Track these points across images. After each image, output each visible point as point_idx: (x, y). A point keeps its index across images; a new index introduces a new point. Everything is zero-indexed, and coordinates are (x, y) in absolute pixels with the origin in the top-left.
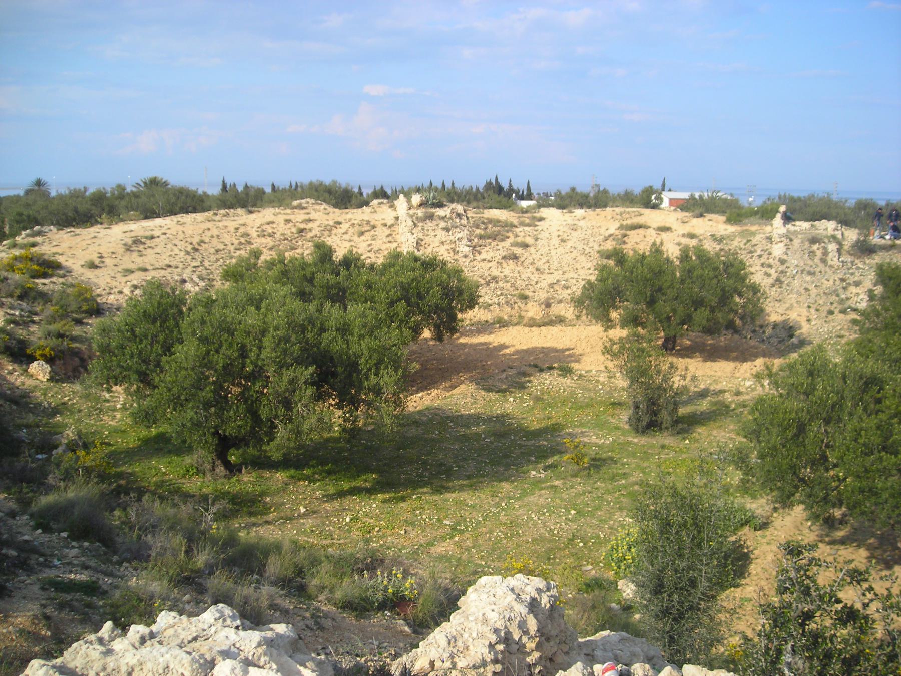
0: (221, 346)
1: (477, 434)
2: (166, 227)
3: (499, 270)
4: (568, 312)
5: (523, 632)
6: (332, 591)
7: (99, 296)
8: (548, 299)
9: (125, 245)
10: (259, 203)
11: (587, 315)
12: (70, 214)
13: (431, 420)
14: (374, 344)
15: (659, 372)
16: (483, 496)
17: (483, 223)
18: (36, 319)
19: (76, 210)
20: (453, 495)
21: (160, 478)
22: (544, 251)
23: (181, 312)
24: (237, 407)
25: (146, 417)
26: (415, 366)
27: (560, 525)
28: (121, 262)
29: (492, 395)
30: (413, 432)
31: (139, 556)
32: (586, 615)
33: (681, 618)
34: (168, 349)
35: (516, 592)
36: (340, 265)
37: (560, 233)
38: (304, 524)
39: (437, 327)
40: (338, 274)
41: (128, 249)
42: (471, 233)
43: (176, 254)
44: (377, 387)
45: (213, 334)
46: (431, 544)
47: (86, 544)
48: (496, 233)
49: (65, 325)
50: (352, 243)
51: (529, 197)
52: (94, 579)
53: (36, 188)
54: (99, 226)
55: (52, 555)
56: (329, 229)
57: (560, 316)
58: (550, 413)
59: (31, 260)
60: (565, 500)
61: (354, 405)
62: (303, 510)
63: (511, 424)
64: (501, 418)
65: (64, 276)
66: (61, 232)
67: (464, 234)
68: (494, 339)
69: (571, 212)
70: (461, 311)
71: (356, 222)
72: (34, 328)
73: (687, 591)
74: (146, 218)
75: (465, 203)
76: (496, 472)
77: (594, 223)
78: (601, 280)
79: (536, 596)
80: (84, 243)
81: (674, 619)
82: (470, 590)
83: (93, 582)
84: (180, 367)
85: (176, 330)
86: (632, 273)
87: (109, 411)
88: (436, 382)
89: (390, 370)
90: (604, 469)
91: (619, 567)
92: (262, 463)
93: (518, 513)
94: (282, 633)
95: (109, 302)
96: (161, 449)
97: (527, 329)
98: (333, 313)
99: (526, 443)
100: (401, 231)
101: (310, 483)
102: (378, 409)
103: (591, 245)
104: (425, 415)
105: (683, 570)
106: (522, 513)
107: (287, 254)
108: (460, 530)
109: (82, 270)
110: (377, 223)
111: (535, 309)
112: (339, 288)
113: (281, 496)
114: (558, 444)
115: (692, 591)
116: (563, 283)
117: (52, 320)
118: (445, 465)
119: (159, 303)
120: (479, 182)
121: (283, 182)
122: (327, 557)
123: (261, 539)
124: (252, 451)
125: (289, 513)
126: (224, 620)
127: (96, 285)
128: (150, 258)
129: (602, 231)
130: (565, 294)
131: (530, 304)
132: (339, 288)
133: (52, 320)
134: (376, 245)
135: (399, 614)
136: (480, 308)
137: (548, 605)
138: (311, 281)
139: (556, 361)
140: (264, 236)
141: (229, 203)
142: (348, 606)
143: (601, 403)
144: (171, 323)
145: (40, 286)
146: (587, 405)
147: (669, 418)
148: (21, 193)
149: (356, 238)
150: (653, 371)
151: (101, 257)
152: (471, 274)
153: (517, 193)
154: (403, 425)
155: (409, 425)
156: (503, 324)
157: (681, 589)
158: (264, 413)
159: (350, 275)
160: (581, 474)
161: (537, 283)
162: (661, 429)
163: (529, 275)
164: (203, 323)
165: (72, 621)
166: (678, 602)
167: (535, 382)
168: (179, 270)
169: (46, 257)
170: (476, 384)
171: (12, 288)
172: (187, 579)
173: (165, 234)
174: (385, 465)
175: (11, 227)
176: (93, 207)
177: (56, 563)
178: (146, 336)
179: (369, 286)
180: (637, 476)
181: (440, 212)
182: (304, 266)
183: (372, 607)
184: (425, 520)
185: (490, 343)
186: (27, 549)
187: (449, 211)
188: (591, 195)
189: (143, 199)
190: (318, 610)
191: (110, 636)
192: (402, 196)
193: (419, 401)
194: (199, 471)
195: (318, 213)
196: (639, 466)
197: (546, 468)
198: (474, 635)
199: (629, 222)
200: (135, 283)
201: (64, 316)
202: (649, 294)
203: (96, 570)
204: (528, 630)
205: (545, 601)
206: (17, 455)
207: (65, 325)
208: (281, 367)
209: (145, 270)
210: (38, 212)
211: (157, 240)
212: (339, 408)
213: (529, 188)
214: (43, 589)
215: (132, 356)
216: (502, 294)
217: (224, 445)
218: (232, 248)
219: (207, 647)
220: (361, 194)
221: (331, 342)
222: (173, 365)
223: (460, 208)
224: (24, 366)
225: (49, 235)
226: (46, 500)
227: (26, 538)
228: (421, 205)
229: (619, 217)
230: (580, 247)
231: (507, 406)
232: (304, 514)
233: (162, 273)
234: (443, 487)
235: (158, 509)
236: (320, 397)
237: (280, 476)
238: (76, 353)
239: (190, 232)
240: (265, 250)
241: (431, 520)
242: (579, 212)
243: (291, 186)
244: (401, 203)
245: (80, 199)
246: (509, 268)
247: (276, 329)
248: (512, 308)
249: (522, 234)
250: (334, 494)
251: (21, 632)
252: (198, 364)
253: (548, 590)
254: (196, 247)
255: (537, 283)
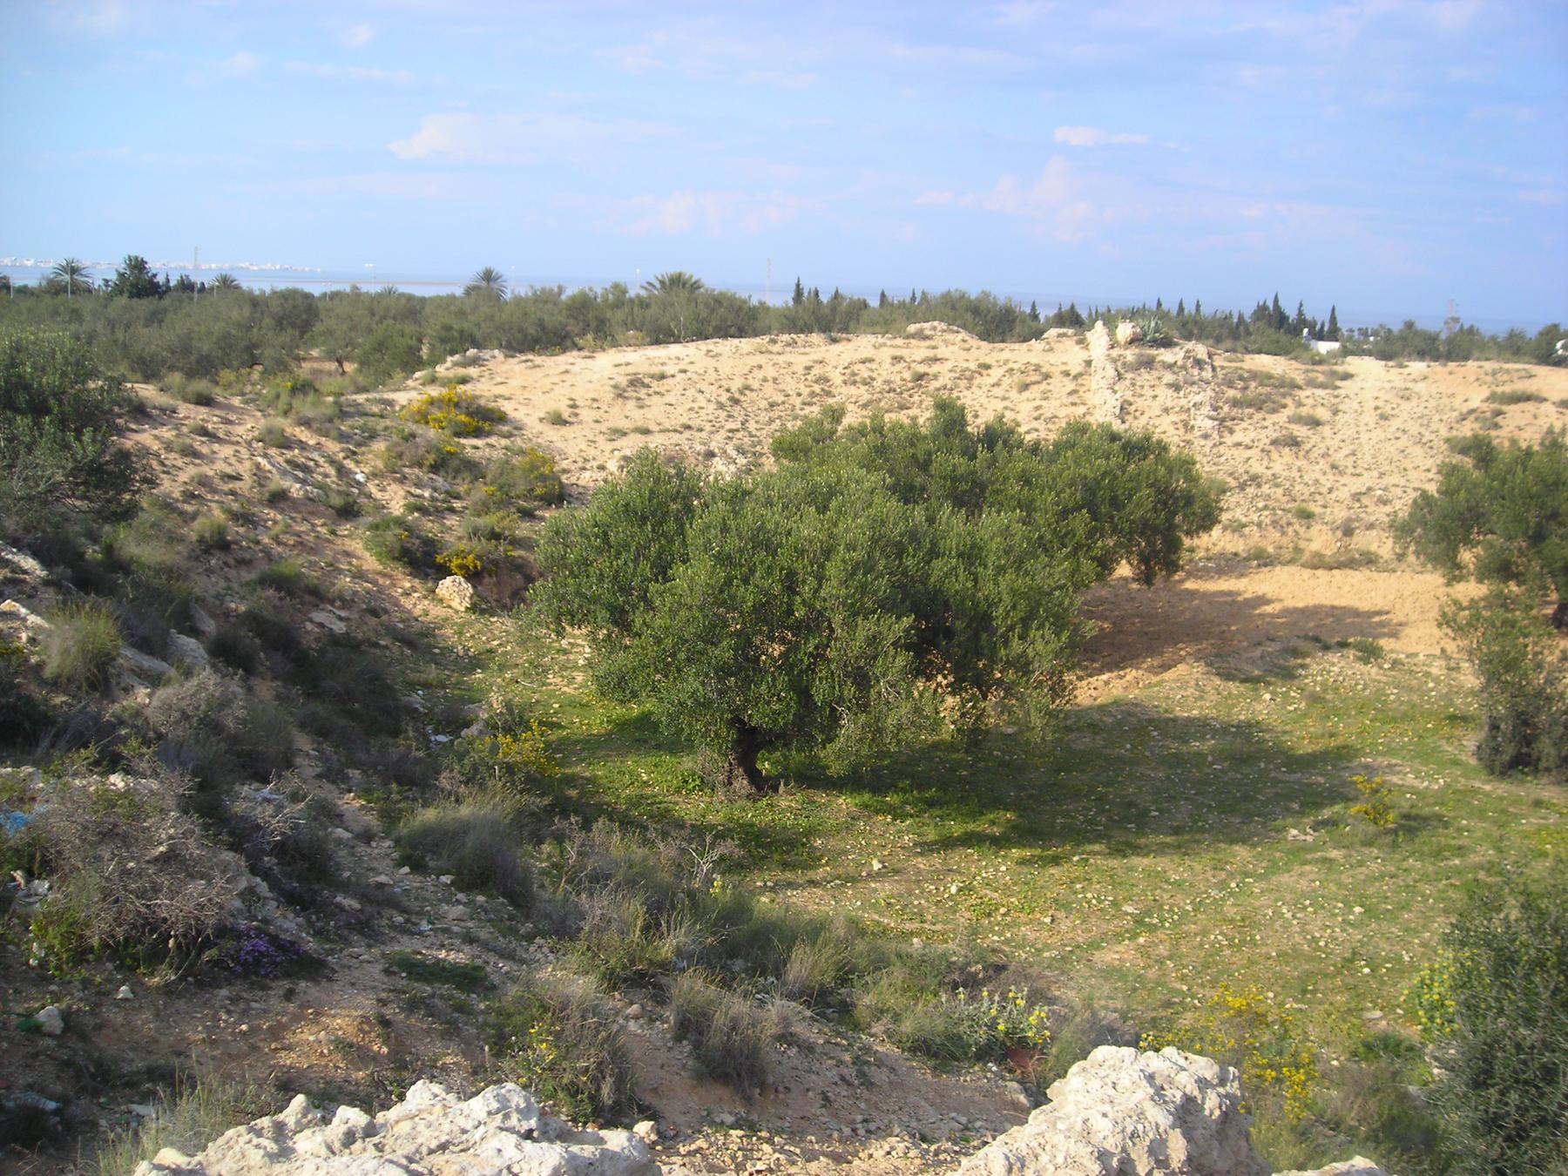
0: (752, 571)
1: (1200, 755)
2: (687, 360)
3: (1265, 463)
4: (1383, 545)
5: (1157, 1161)
6: (897, 1018)
7: (565, 471)
8: (1349, 520)
9: (615, 387)
10: (852, 325)
11: (1417, 553)
12: (531, 331)
13: (1120, 723)
14: (1022, 583)
15: (1539, 666)
16: (1197, 867)
17: (1241, 378)
18: (457, 505)
19: (541, 325)
20: (1146, 861)
21: (638, 792)
22: (1347, 433)
23: (689, 509)
24: (774, 679)
25: (618, 685)
26: (1091, 628)
27: (1331, 931)
28: (606, 416)
29: (1234, 687)
30: (1084, 742)
31: (563, 930)
32: (1360, 1100)
33: (1522, 1138)
34: (662, 571)
35: (1158, 1082)
36: (979, 440)
37: (1380, 403)
38: (875, 890)
39: (1144, 559)
40: (973, 457)
41: (620, 394)
42: (1218, 395)
43: (696, 408)
44: (1023, 660)
45: (741, 551)
46: (1094, 945)
47: (481, 899)
48: (1263, 397)
49: (503, 519)
50: (1007, 403)
51: (1333, 334)
52: (479, 962)
53: (484, 284)
54: (575, 353)
55: (421, 913)
56: (968, 377)
57: (1369, 553)
58: (1335, 725)
59: (457, 405)
60: (1345, 887)
61: (980, 689)
62: (876, 866)
63: (1262, 741)
64: (1245, 730)
65: (508, 436)
66: (511, 360)
67: (1205, 396)
68: (1247, 586)
69: (1401, 366)
70: (1188, 533)
71: (1015, 366)
72: (452, 521)
73: (1537, 1087)
74: (657, 342)
75: (1211, 341)
76: (1226, 826)
77: (1442, 389)
78: (1447, 492)
79: (1196, 1093)
80: (547, 381)
81: (1508, 1139)
82: (1075, 1068)
83: (476, 968)
84: (679, 603)
85: (678, 540)
86: (1504, 481)
87: (557, 672)
88: (1135, 657)
89: (1047, 632)
90: (1423, 836)
91: (1431, 1019)
92: (813, 778)
93: (1257, 903)
94: (617, 1149)
95: (580, 483)
96: (646, 741)
97: (1307, 573)
98: (954, 525)
99: (1288, 777)
100: (1094, 386)
101: (894, 819)
102: (1021, 699)
103: (1434, 426)
104: (1110, 714)
105: (1533, 1047)
106: (1264, 905)
107: (887, 418)
108: (1150, 924)
109: (540, 427)
110: (1053, 369)
111: (1324, 537)
112: (974, 482)
113: (843, 838)
114: (1344, 784)
115: (1547, 1089)
116: (1379, 492)
117: (484, 508)
118: (1136, 806)
119: (652, 492)
120: (1243, 303)
121: (900, 291)
122: (899, 956)
123: (787, 910)
124: (797, 757)
125: (851, 870)
126: (507, 1117)
127: (562, 453)
128: (655, 413)
129: (1457, 403)
130: (1380, 514)
131: (1315, 529)
132: (974, 482)
133: (484, 508)
134: (1049, 408)
135: (1011, 1071)
136: (1225, 529)
137: (1217, 1113)
138: (924, 466)
139: (1355, 633)
140: (854, 383)
141: (801, 323)
142: (922, 1047)
143: (1430, 715)
144: (671, 526)
145: (468, 450)
146: (1405, 717)
147: (1553, 752)
148: (459, 292)
149: (1014, 394)
150: (1528, 663)
151: (574, 406)
152: (1214, 468)
153: (1312, 326)
154: (1068, 729)
155: (1079, 729)
156: (1264, 560)
157: (1526, 1083)
158: (820, 692)
159: (994, 460)
160: (1380, 841)
161: (1331, 490)
162: (1537, 770)
163: (1318, 475)
164: (725, 529)
165: (428, 1032)
166: (1518, 1108)
167: (1314, 668)
168: (703, 435)
169: (482, 402)
170: (1207, 665)
171: (421, 451)
172: (641, 975)
173: (685, 371)
174: (1031, 796)
175: (433, 348)
176: (571, 321)
177: (425, 926)
178: (626, 546)
179: (1026, 480)
180: (1488, 853)
181: (1166, 355)
182: (914, 439)
183: (966, 1053)
184: (1089, 902)
185: (1238, 593)
186: (379, 898)
187: (1182, 354)
188: (1443, 336)
189: (654, 310)
190: (867, 1049)
191: (298, 1122)
192: (1099, 324)
193: (1096, 690)
194: (705, 784)
195: (951, 348)
196: (1488, 836)
197: (1316, 826)
198: (1060, 1160)
199: (1508, 388)
200: (628, 453)
201: (504, 502)
202: (1533, 521)
203: (487, 947)
204: (1167, 1159)
205: (1212, 1104)
206: (396, 732)
207: (503, 519)
208: (856, 614)
209: (647, 432)
210: (478, 325)
211: (670, 381)
212: (953, 693)
213: (1333, 319)
214: (387, 972)
215: (601, 577)
216: (1266, 507)
217: (748, 743)
218: (798, 402)
219: (456, 1167)
220: (1035, 317)
221: (946, 575)
222: (668, 599)
223: (1201, 350)
224: (430, 584)
225: (491, 365)
226: (429, 815)
227: (383, 879)
228: (1131, 342)
229: (1489, 379)
230: (1414, 428)
231: (1259, 707)
232: (878, 873)
233: (676, 437)
234: (1128, 845)
235: (615, 846)
236: (922, 669)
237: (845, 803)
238: (519, 567)
239: (728, 371)
240: (850, 407)
241: (1100, 902)
242: (1417, 367)
243: (913, 298)
244: (1098, 335)
245: (550, 306)
246: (1282, 462)
247: (851, 547)
248: (1284, 534)
249: (1310, 401)
250: (936, 842)
251: (343, 1046)
252: (711, 600)
253: (1223, 1082)
254: (737, 395)
255: (1331, 490)
